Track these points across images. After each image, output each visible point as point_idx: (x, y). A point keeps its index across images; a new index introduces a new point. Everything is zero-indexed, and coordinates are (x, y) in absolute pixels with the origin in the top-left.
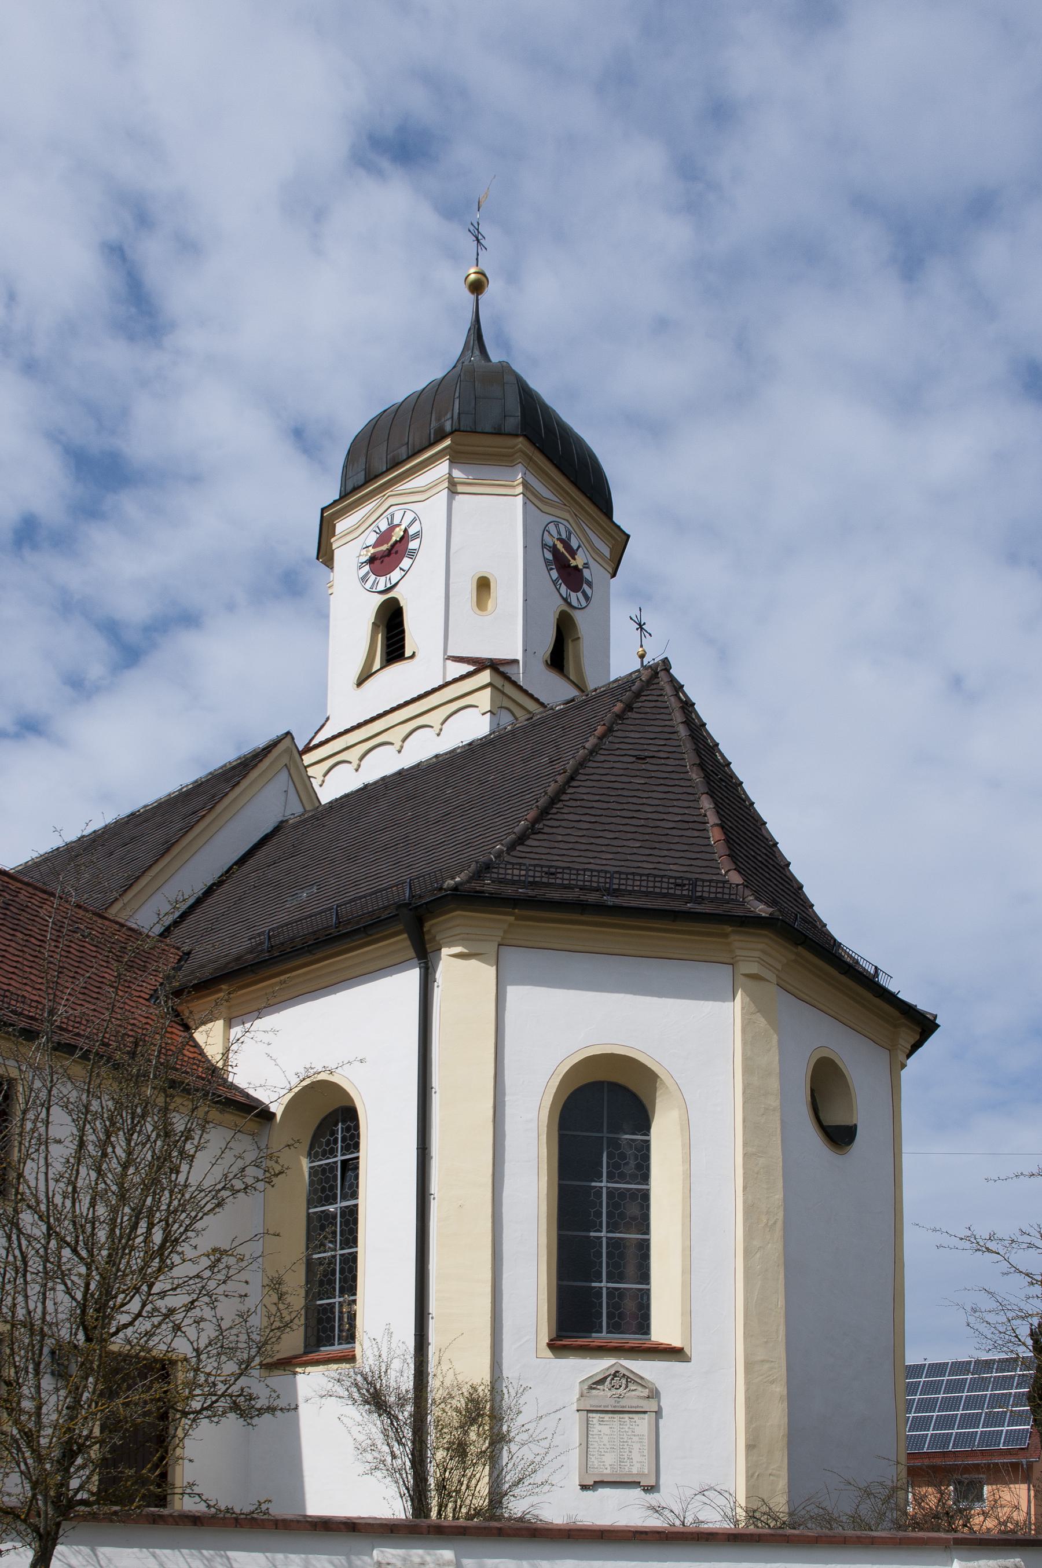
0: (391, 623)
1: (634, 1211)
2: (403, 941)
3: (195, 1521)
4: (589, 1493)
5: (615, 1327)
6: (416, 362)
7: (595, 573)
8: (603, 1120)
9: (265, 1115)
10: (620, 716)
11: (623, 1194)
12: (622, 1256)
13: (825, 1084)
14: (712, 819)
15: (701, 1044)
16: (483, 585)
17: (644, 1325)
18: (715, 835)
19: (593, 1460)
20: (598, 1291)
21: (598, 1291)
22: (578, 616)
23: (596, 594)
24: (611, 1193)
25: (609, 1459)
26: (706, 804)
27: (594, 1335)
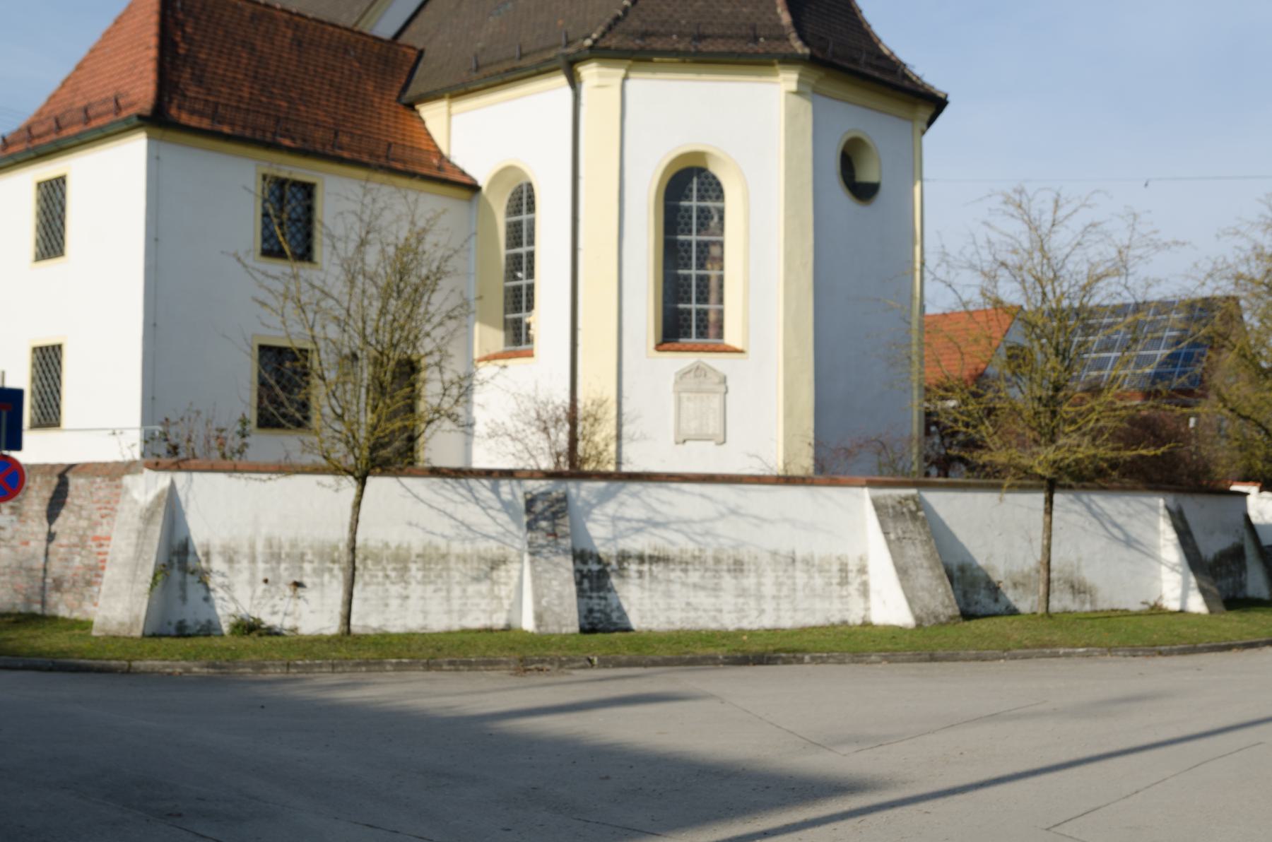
1: (710, 254)
4: (680, 447)
5: (702, 333)
8: (689, 197)
12: (707, 286)
15: (753, 125)
17: (720, 335)
20: (686, 313)
21: (686, 313)
24: (698, 244)
27: (682, 340)
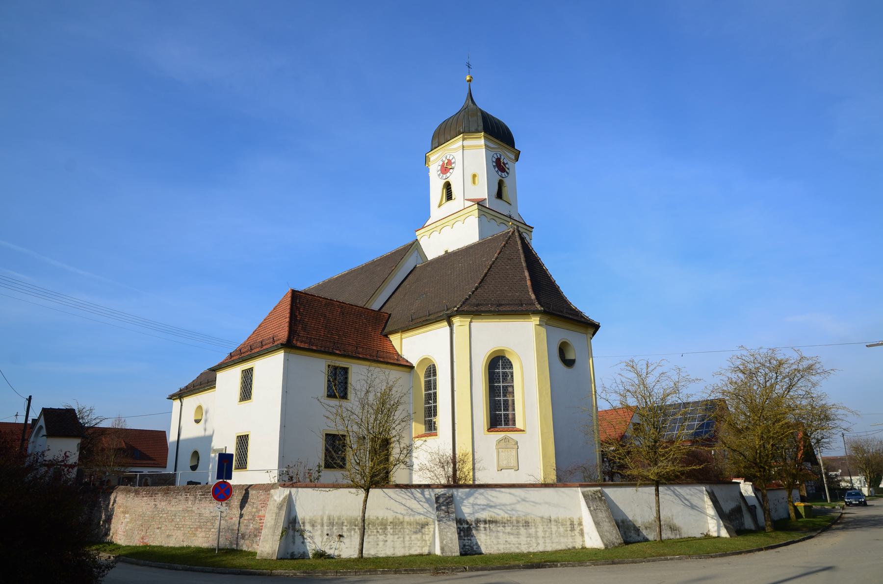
0: (448, 186)
1: (508, 390)
2: (446, 323)
3: (398, 486)
5: (507, 424)
6: (454, 106)
7: (510, 165)
8: (498, 368)
9: (411, 367)
10: (504, 246)
11: (507, 387)
13: (563, 350)
14: (528, 278)
16: (474, 176)
17: (514, 424)
18: (529, 283)
19: (501, 463)
20: (500, 415)
21: (500, 415)
22: (505, 180)
23: (511, 172)
25: (505, 462)
26: (527, 274)
